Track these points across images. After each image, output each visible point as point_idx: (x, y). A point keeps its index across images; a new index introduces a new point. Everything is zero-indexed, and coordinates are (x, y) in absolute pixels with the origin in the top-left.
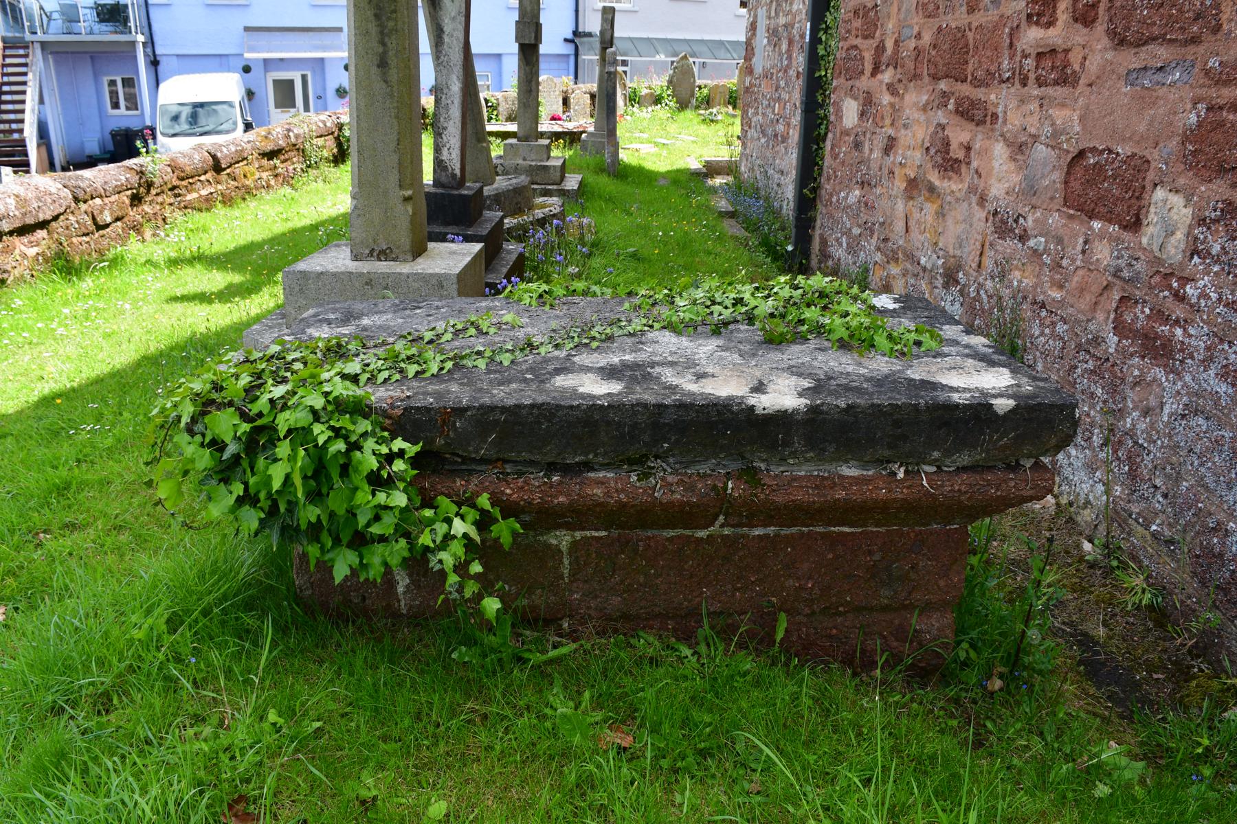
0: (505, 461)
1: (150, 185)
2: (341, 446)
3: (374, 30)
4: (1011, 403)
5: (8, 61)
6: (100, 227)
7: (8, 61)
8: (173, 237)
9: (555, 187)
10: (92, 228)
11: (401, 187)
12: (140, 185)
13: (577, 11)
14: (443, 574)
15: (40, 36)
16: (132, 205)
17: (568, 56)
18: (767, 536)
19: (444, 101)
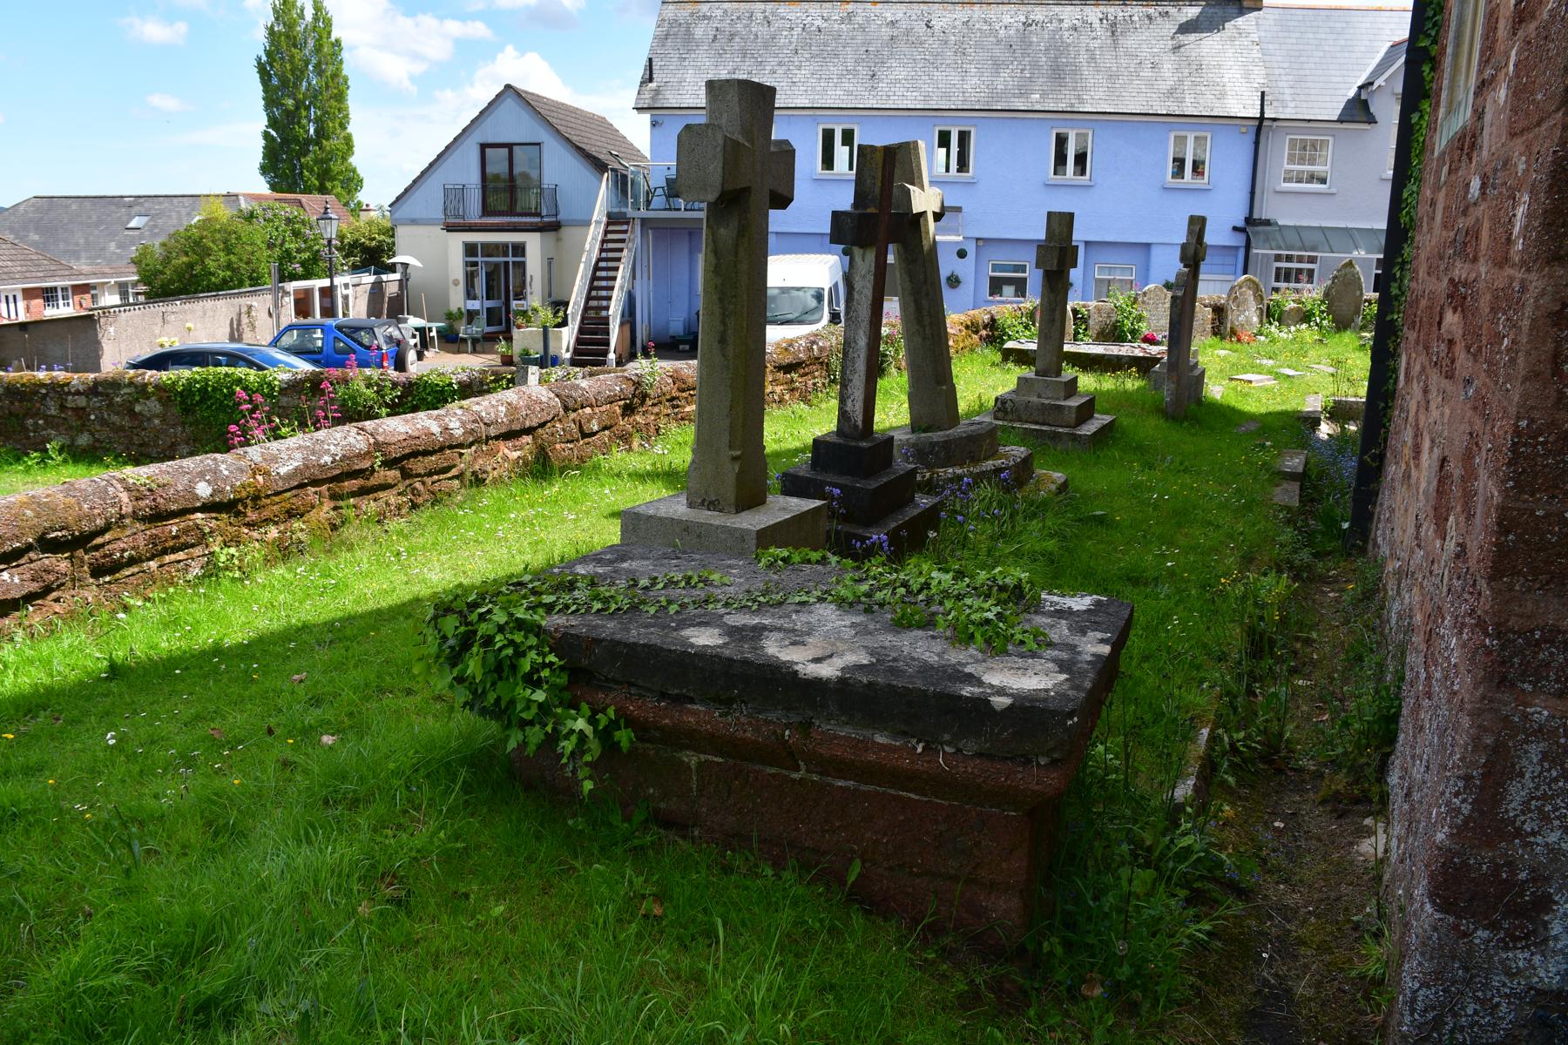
0: (631, 684)
1: (645, 396)
2: (510, 651)
3: (717, 311)
4: (1007, 701)
5: (610, 236)
6: (584, 435)
7: (610, 236)
8: (658, 449)
9: (1066, 430)
10: (577, 435)
11: (731, 448)
12: (634, 396)
13: (1252, 193)
14: (562, 755)
15: (643, 213)
16: (623, 415)
17: (1237, 248)
18: (847, 788)
19: (851, 355)
